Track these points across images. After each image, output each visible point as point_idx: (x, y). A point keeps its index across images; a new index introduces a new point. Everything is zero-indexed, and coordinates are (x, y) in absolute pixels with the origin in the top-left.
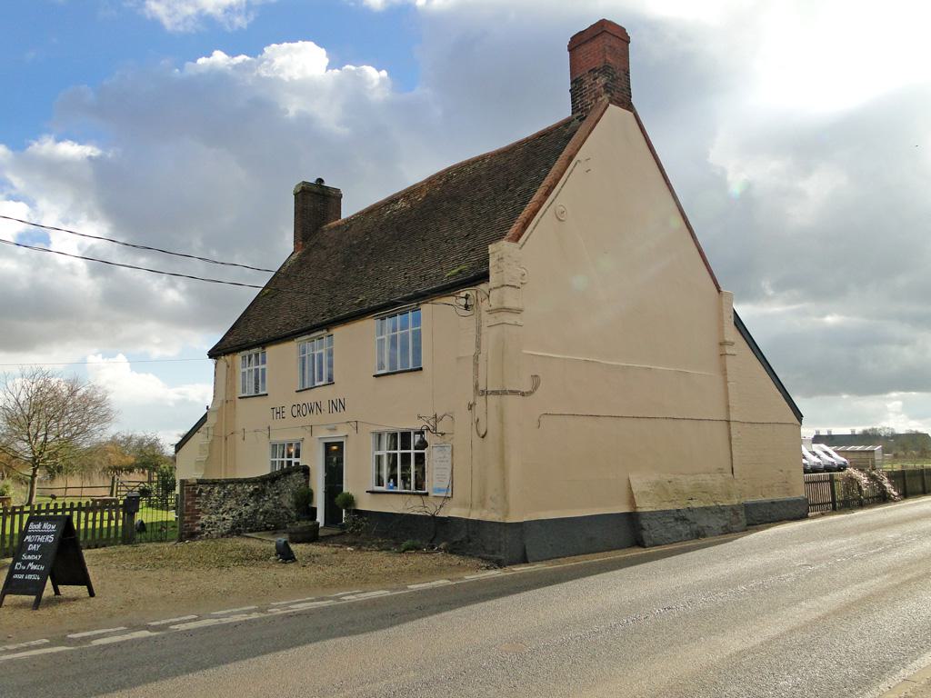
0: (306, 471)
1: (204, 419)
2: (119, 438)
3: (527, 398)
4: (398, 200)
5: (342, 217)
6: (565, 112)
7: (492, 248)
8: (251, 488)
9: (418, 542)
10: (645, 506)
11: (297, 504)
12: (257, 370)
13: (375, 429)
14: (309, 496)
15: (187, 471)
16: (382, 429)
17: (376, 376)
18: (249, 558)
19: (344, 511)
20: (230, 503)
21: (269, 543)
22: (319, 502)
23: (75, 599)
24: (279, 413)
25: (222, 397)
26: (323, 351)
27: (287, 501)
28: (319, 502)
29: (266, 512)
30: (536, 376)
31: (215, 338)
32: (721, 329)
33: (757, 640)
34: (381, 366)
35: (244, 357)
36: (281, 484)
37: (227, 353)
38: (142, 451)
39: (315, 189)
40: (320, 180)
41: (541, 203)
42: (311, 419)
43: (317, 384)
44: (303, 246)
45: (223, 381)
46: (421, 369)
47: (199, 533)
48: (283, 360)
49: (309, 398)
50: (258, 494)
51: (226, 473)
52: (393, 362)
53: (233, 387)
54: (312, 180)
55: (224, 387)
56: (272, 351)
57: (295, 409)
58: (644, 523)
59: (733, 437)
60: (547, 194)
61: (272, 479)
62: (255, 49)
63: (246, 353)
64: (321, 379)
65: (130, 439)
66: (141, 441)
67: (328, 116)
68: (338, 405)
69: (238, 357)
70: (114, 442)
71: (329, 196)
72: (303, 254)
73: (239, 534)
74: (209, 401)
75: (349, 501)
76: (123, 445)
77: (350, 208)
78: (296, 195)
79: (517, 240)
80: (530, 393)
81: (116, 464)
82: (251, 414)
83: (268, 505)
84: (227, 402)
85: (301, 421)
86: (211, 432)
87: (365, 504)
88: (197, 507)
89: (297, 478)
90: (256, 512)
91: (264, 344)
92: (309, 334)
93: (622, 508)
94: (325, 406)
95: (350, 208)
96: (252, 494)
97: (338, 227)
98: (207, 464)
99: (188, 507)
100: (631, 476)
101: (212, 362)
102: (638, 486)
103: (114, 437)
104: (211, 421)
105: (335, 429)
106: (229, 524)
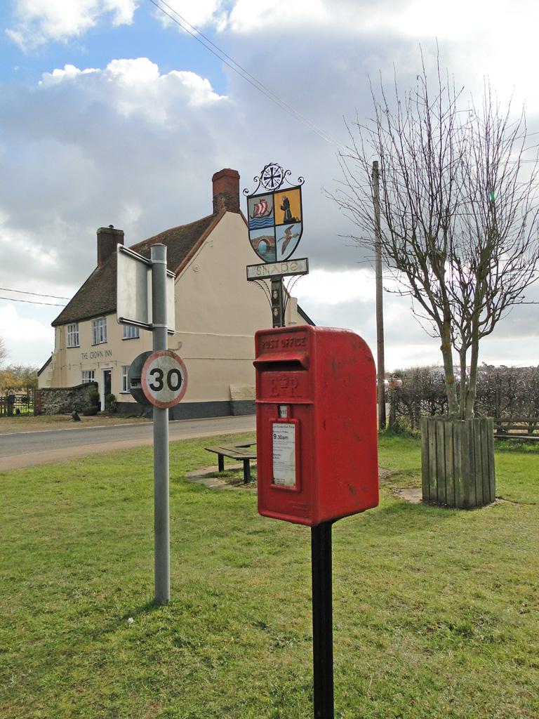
0: (96, 385)
1: (50, 360)
2: (12, 368)
4: (145, 244)
6: (210, 212)
8: (69, 392)
9: (135, 414)
10: (236, 398)
11: (92, 400)
12: (75, 334)
13: (123, 365)
14: (98, 397)
15: (43, 383)
16: (125, 365)
17: (123, 340)
18: (64, 420)
20: (58, 399)
21: (70, 416)
22: (102, 400)
24: (85, 356)
25: (58, 347)
26: (102, 326)
27: (87, 398)
28: (102, 400)
29: (76, 404)
31: (56, 313)
34: (125, 335)
35: (69, 327)
36: (83, 390)
37: (59, 325)
38: (28, 377)
39: (109, 232)
40: (111, 226)
41: (185, 265)
42: (98, 359)
44: (102, 264)
45: (59, 339)
47: (43, 412)
48: (86, 328)
49: (97, 349)
50: (72, 395)
51: (60, 384)
52: (134, 335)
53: (64, 342)
55: (60, 340)
56: (81, 325)
57: (92, 355)
58: (235, 405)
60: (189, 260)
61: (79, 388)
62: (103, 64)
63: (69, 325)
65: (19, 369)
66: (27, 371)
67: (158, 116)
68: (109, 353)
69: (66, 327)
70: (9, 371)
71: (116, 235)
72: (101, 270)
73: (63, 413)
74: (52, 348)
75: (113, 398)
76: (15, 373)
78: (98, 234)
81: (10, 385)
82: (73, 356)
83: (77, 401)
85: (95, 360)
87: (120, 399)
88: (42, 401)
89: (92, 388)
90: (71, 403)
91: (77, 321)
93: (227, 399)
94: (104, 354)
96: (69, 395)
98: (52, 382)
99: (38, 401)
100: (231, 385)
101: (53, 329)
102: (234, 388)
103: (8, 368)
105: (108, 365)
106: (58, 408)
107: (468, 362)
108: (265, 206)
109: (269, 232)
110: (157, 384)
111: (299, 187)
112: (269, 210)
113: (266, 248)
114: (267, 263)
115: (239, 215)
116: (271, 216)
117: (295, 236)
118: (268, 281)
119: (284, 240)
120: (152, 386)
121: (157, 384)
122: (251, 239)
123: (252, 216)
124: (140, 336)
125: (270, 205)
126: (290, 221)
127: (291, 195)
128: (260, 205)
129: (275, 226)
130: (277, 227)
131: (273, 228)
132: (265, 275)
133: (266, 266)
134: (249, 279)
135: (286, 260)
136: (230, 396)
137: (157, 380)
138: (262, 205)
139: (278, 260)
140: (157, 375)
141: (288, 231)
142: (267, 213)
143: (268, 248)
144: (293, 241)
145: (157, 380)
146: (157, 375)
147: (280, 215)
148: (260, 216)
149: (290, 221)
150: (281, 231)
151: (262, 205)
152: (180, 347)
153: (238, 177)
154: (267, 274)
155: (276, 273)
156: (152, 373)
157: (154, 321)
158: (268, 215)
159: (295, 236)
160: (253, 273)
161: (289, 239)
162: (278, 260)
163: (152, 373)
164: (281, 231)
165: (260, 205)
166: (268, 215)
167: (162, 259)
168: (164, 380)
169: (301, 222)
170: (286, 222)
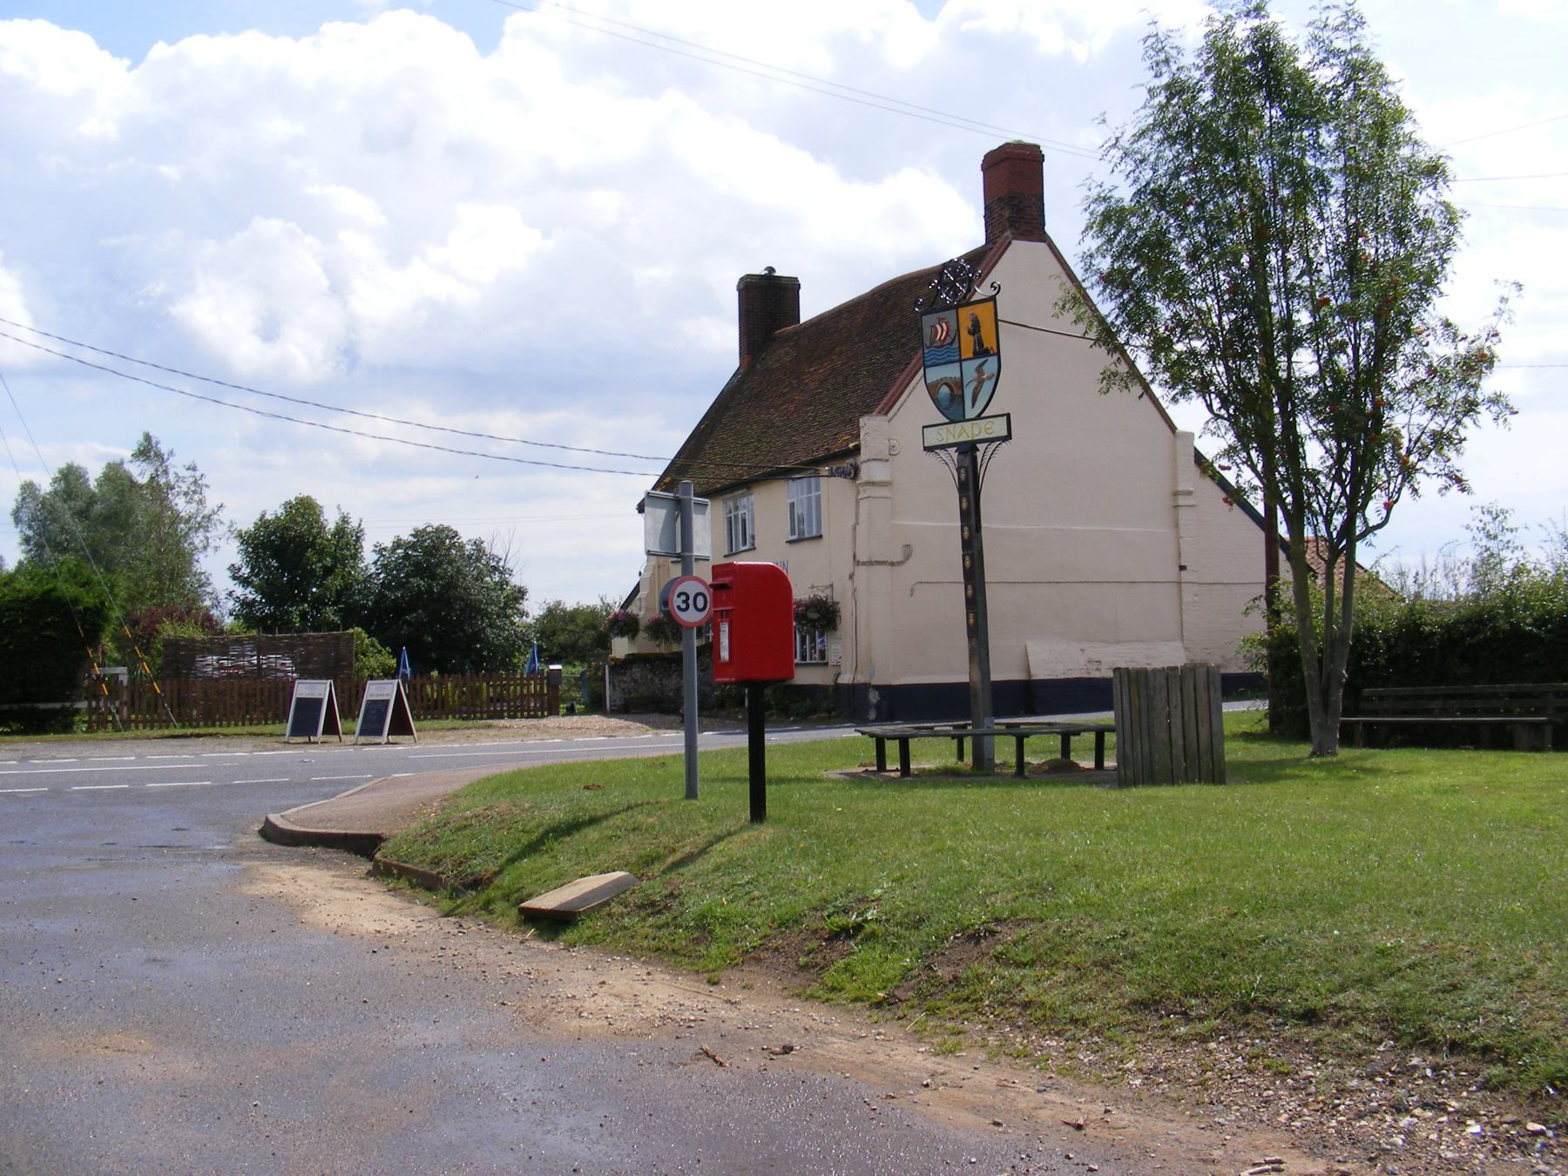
1: (636, 590)
3: (908, 563)
5: (803, 319)
7: (862, 421)
9: (1444, 804)
17: (790, 542)
19: (725, 655)
23: (572, 828)
30: (908, 546)
32: (1174, 477)
33: (1290, 756)
34: (793, 532)
40: (771, 270)
43: (742, 548)
46: (821, 536)
54: (759, 270)
59: (1184, 600)
64: (745, 543)
77: (810, 308)
79: (886, 414)
80: (900, 563)
84: (659, 567)
86: (643, 602)
92: (732, 492)
95: (810, 308)
97: (796, 333)
101: (641, 517)
104: (642, 594)
107: (1338, 590)
108: (945, 328)
109: (951, 371)
110: (683, 606)
111: (993, 299)
112: (952, 334)
113: (948, 397)
114: (952, 422)
115: (1044, 245)
116: (956, 345)
117: (989, 378)
118: (952, 450)
119: (974, 384)
120: (679, 607)
121: (683, 606)
122: (928, 382)
123: (928, 344)
124: (824, 532)
125: (953, 324)
126: (981, 352)
127: (984, 312)
128: (938, 326)
129: (961, 361)
130: (958, 364)
131: (958, 364)
132: (950, 442)
133: (951, 427)
134: (928, 449)
135: (979, 417)
136: (1029, 671)
137: (683, 602)
138: (942, 327)
139: (967, 417)
140: (684, 597)
141: (979, 369)
142: (948, 341)
143: (953, 397)
144: (987, 386)
145: (683, 602)
146: (684, 597)
147: (967, 342)
148: (939, 344)
149: (981, 352)
150: (970, 367)
151: (942, 327)
152: (908, 557)
153: (1041, 158)
154: (951, 440)
155: (964, 438)
156: (679, 596)
157: (683, 551)
158: (951, 343)
159: (989, 378)
160: (933, 437)
161: (981, 382)
162: (967, 417)
163: (679, 596)
164: (970, 367)
165: (938, 326)
166: (951, 343)
167: (690, 494)
168: (691, 602)
169: (998, 354)
170: (977, 355)
